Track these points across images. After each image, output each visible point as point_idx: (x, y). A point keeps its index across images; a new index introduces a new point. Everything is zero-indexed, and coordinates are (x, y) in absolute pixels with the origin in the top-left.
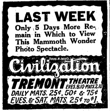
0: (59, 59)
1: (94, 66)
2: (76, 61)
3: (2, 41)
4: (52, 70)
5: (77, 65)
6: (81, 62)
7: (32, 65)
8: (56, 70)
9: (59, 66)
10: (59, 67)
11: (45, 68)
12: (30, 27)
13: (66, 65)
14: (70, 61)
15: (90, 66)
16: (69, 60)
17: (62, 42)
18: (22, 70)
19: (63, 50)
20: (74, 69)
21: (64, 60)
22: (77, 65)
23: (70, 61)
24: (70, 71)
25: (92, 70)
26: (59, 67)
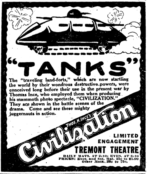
0: (78, 120)
1: (127, 110)
2: (101, 114)
3: (138, 91)
4: (76, 137)
5: (105, 118)
6: (108, 112)
7: (48, 144)
8: (81, 136)
9: (82, 129)
10: (83, 131)
11: (66, 139)
12: (37, 85)
13: (91, 124)
14: (93, 116)
15: (121, 112)
16: (92, 116)
17: (36, 100)
18: (38, 154)
19: (106, 99)
20: (110, 122)
21: (85, 119)
22: (105, 118)
23: (93, 116)
24: (70, 142)
25: (126, 117)
26: (83, 131)
